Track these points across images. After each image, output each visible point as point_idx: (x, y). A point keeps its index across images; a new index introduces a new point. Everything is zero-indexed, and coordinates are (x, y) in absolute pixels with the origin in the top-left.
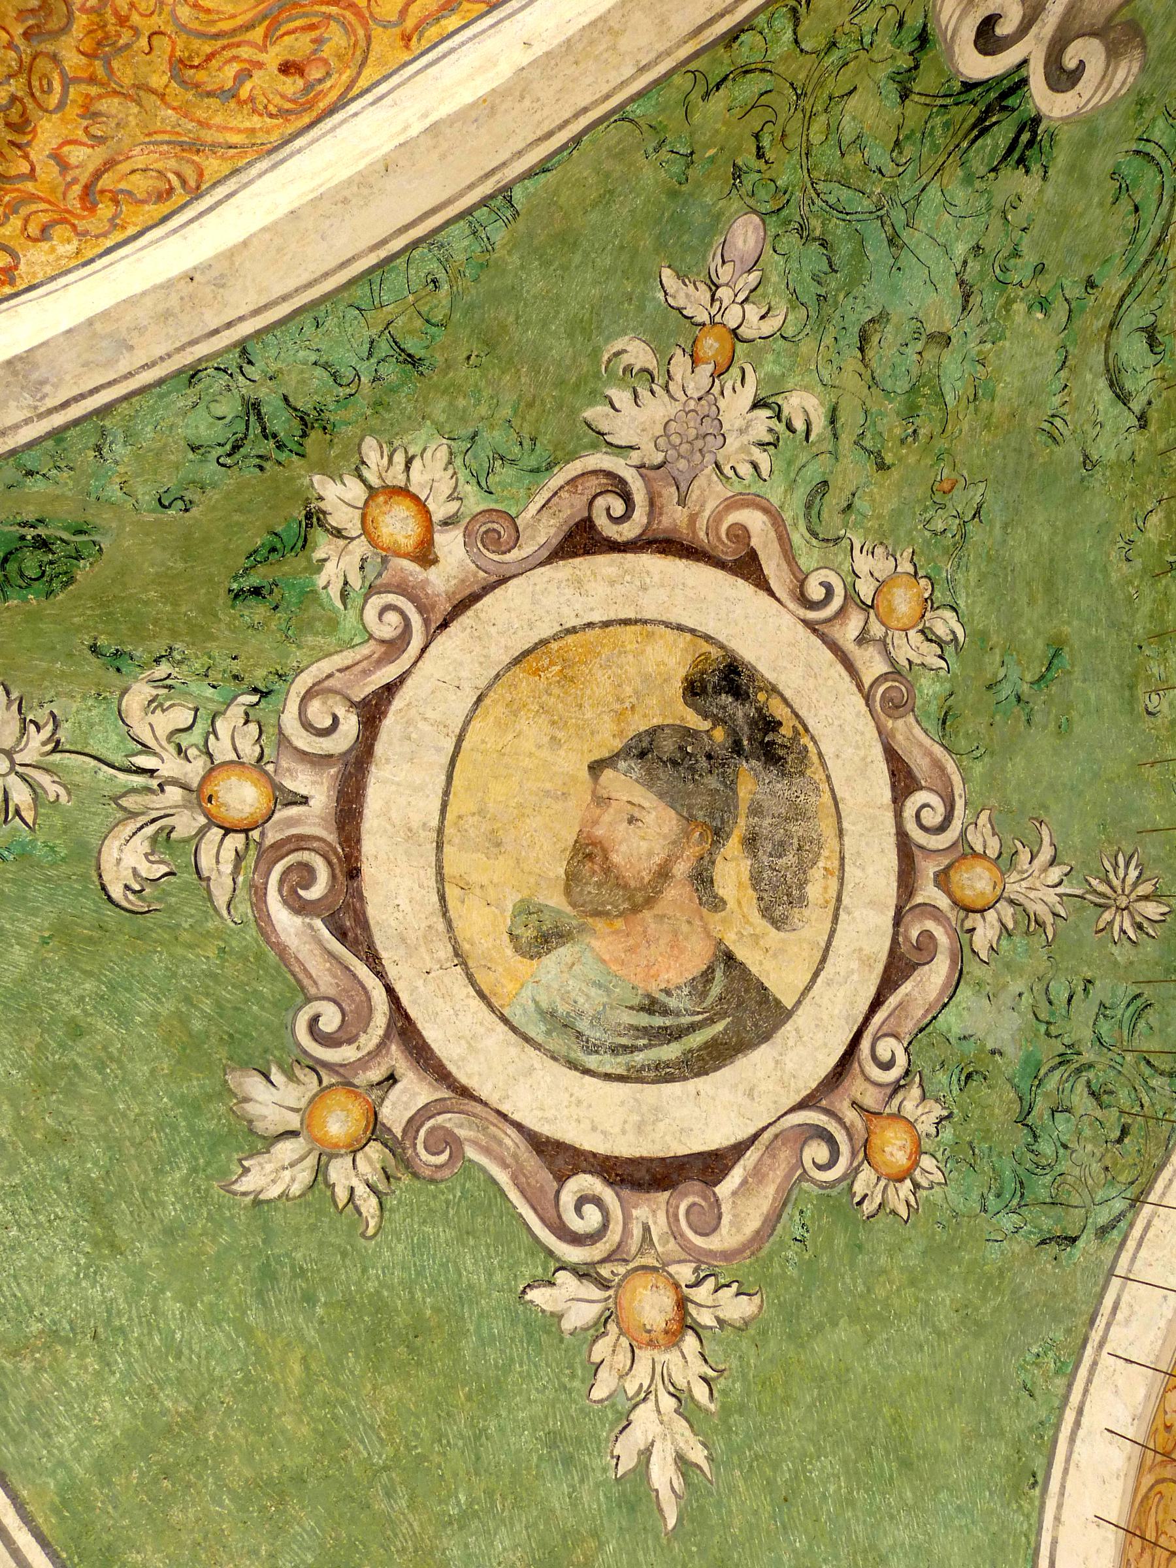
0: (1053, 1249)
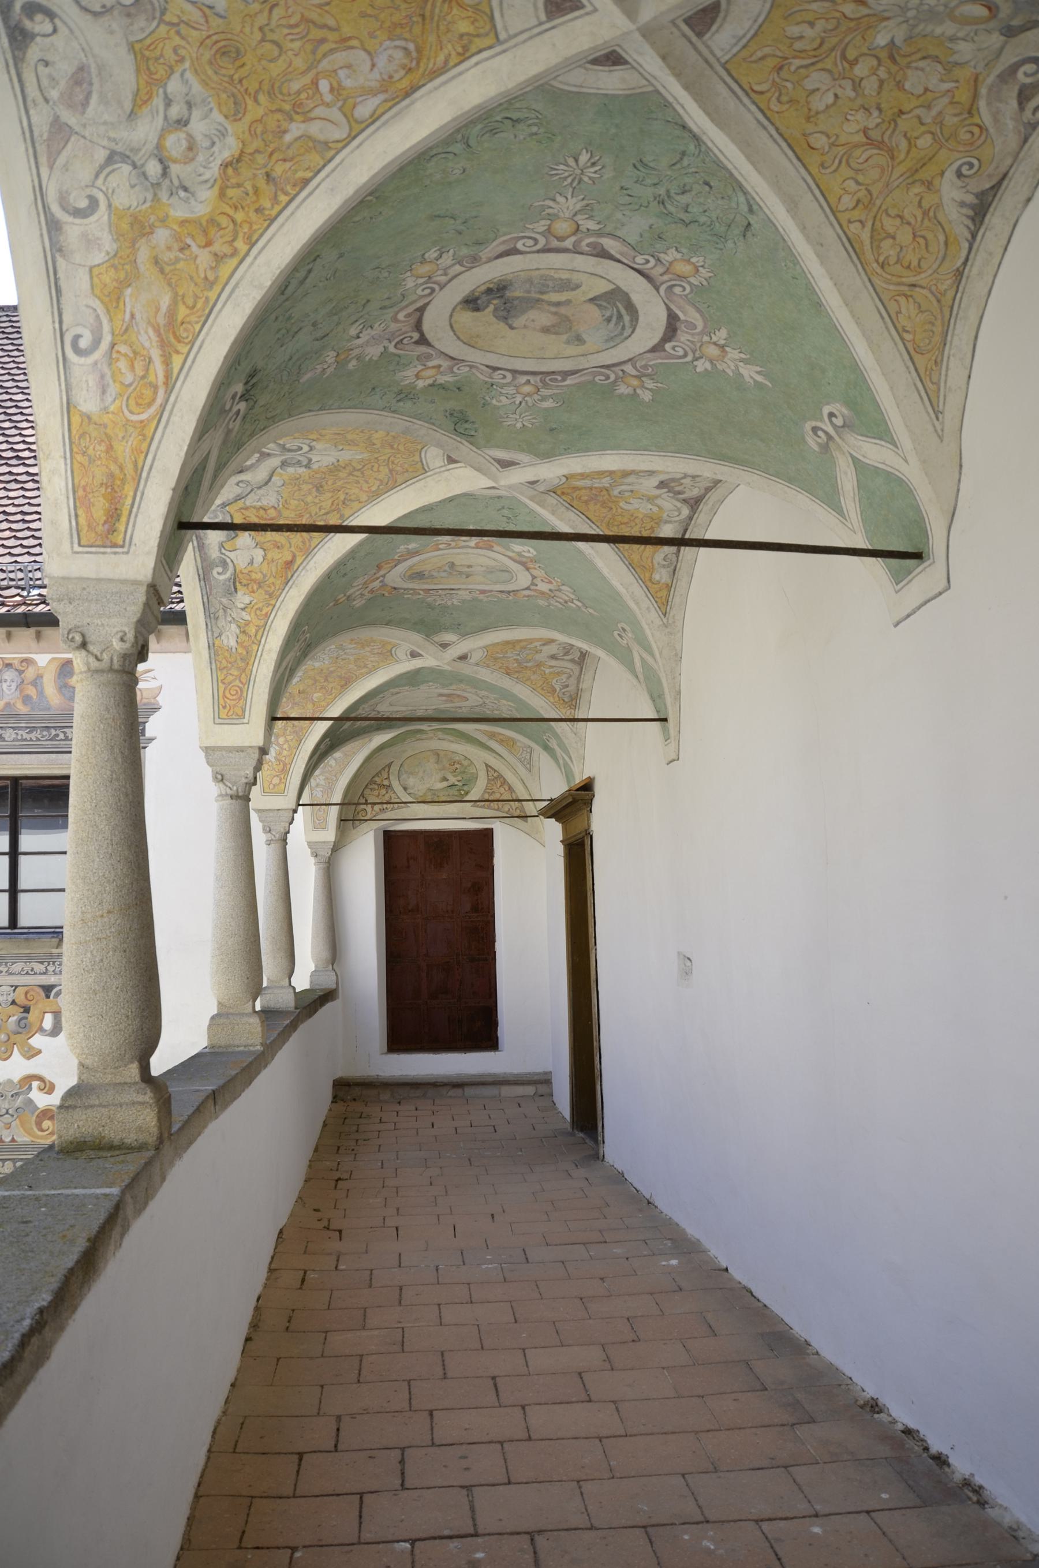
0: (749, 234)
